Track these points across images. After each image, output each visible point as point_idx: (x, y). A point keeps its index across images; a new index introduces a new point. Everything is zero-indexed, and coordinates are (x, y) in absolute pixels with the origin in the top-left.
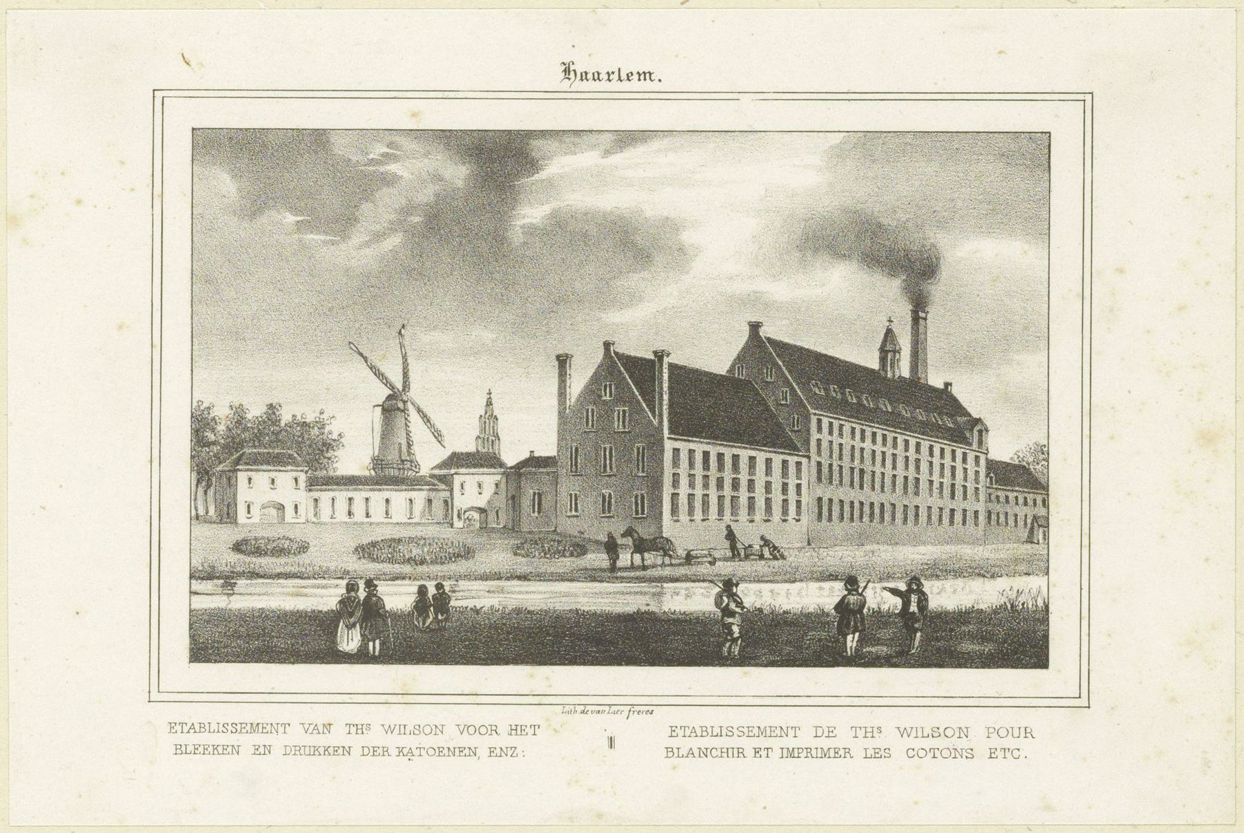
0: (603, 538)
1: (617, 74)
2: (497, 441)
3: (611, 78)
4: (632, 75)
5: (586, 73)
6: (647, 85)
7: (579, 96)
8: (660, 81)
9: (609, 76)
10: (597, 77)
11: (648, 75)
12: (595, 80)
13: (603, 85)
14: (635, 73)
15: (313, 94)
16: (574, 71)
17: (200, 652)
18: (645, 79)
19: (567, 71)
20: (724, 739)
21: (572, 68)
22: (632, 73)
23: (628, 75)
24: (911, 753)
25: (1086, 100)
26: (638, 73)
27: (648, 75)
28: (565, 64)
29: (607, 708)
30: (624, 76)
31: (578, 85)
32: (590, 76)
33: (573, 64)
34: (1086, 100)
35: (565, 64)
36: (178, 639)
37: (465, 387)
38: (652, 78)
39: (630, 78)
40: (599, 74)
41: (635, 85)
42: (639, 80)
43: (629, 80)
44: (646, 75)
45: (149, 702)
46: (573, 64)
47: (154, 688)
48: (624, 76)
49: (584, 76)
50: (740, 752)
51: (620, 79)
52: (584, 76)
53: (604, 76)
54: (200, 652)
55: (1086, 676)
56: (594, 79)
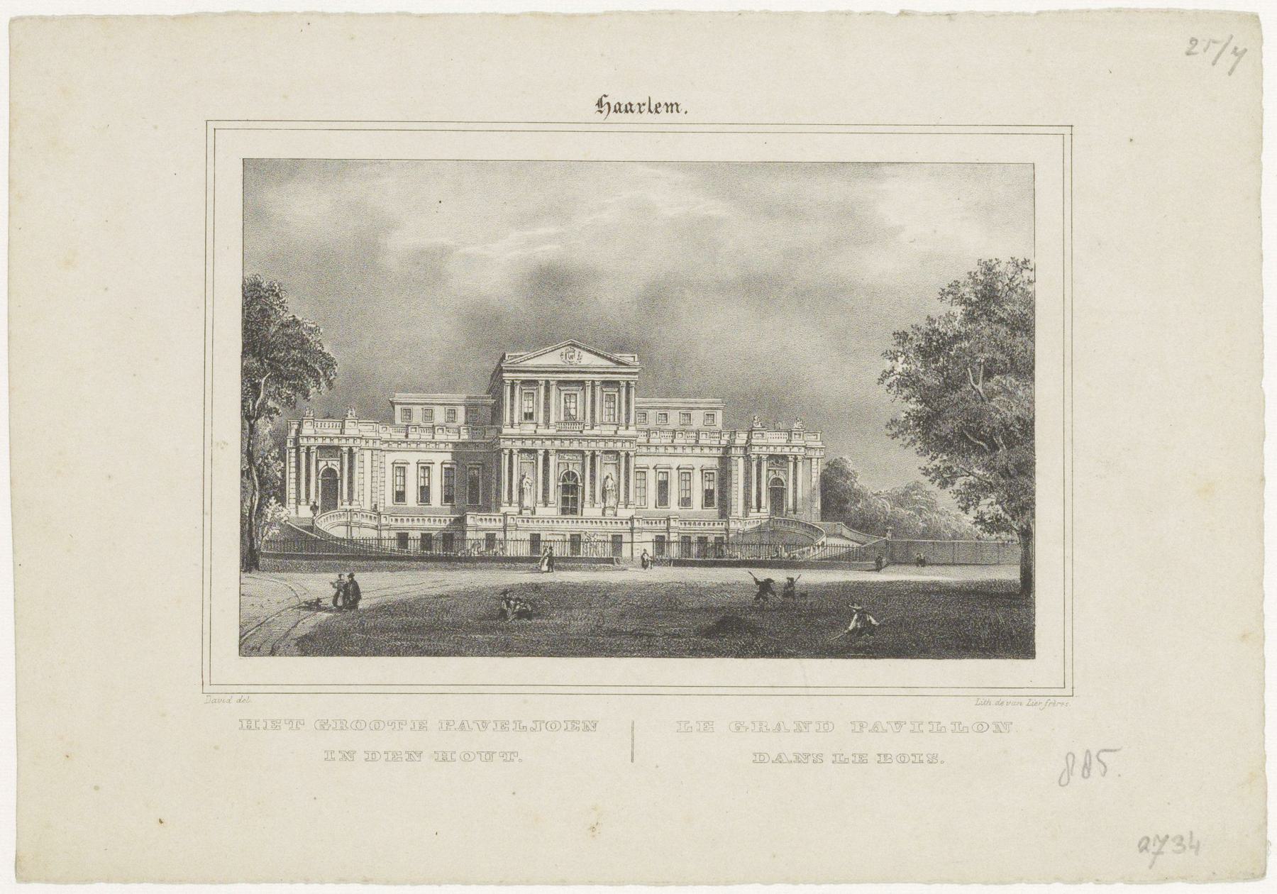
0: (1153, 856)
1: (647, 104)
3: (642, 110)
4: (660, 105)
5: (620, 105)
9: (259, 648)
11: (675, 107)
12: (676, 104)
14: (662, 104)
16: (608, 104)
17: (248, 647)
18: (672, 111)
20: (386, 479)
21: (605, 100)
22: (659, 104)
23: (656, 105)
24: (1064, 781)
26: (666, 104)
27: (675, 107)
29: (1025, 700)
30: (653, 108)
32: (623, 108)
34: (212, 127)
37: (986, 348)
39: (658, 109)
42: (667, 111)
43: (658, 113)
48: (653, 108)
51: (650, 110)
53: (635, 108)
54: (248, 647)
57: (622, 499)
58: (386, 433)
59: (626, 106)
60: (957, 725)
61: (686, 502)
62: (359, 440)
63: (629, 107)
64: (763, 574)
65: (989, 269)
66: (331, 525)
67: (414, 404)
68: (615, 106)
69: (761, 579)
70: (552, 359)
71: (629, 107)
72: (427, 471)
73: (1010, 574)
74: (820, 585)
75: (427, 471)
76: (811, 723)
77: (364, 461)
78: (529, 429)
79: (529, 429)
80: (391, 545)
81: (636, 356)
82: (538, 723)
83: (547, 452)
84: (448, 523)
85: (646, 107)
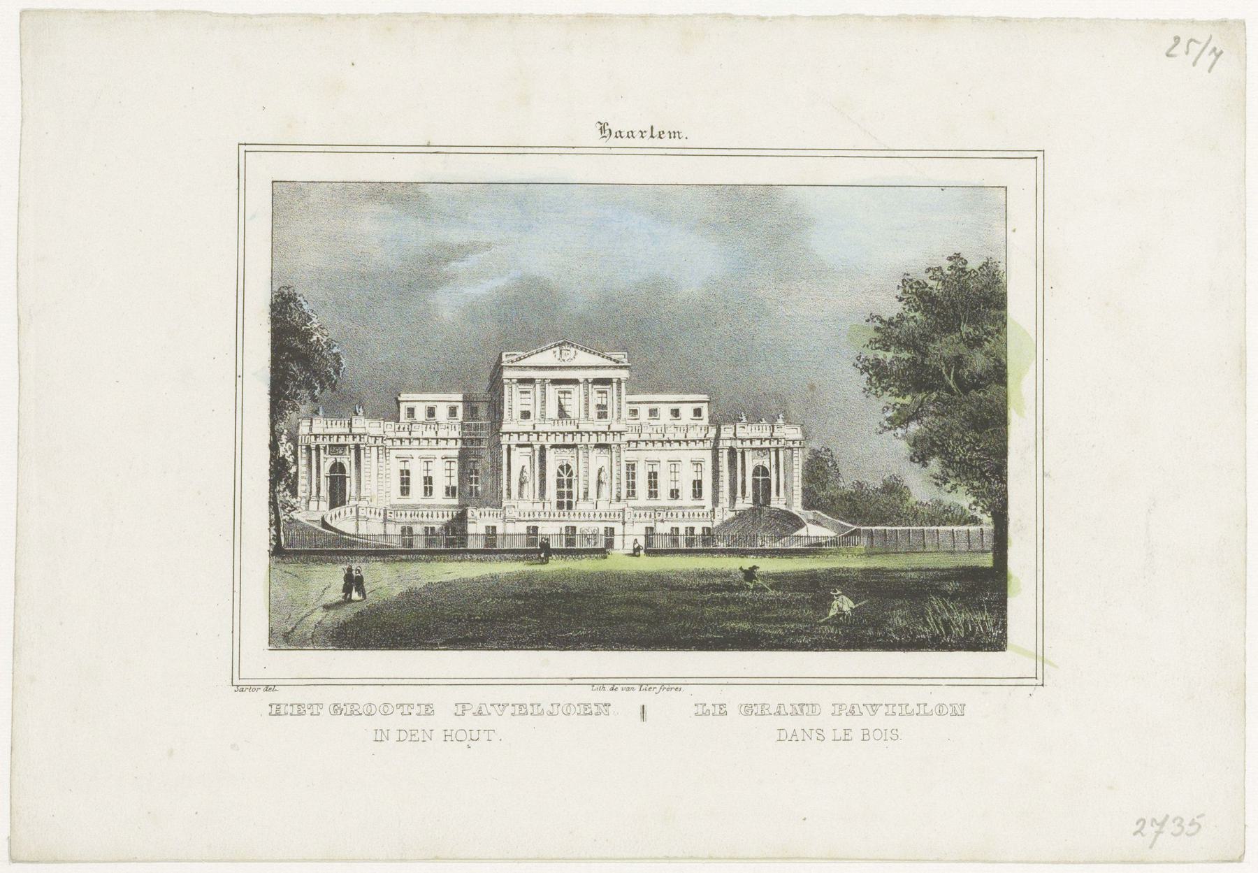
2: (576, 481)
6: (675, 142)
7: (609, 151)
8: (686, 138)
10: (631, 134)
12: (678, 132)
13: (637, 141)
14: (666, 132)
15: (758, 153)
16: (610, 130)
18: (674, 137)
19: (602, 130)
21: (607, 128)
25: (246, 148)
28: (601, 124)
31: (613, 141)
33: (608, 125)
35: (601, 124)
36: (257, 623)
38: (622, 135)
39: (662, 136)
40: (620, 132)
41: (666, 141)
42: (670, 138)
43: (661, 138)
44: (674, 134)
45: (245, 151)
46: (608, 125)
47: (248, 148)
48: (656, 133)
49: (619, 134)
50: (722, 710)
52: (619, 134)
55: (1040, 658)
56: (674, 133)
57: (314, 493)
58: (390, 429)
59: (616, 133)
60: (904, 706)
61: (674, 494)
62: (604, 435)
63: (630, 134)
64: (747, 563)
65: (906, 282)
66: (344, 523)
67: (639, 403)
68: (616, 133)
69: (746, 567)
70: (548, 358)
71: (630, 134)
72: (699, 466)
73: (987, 561)
74: (801, 571)
75: (699, 466)
76: (882, 705)
77: (370, 461)
78: (527, 426)
79: (527, 426)
80: (396, 543)
81: (626, 353)
82: (837, 706)
83: (543, 448)
84: (450, 518)
85: (649, 134)
